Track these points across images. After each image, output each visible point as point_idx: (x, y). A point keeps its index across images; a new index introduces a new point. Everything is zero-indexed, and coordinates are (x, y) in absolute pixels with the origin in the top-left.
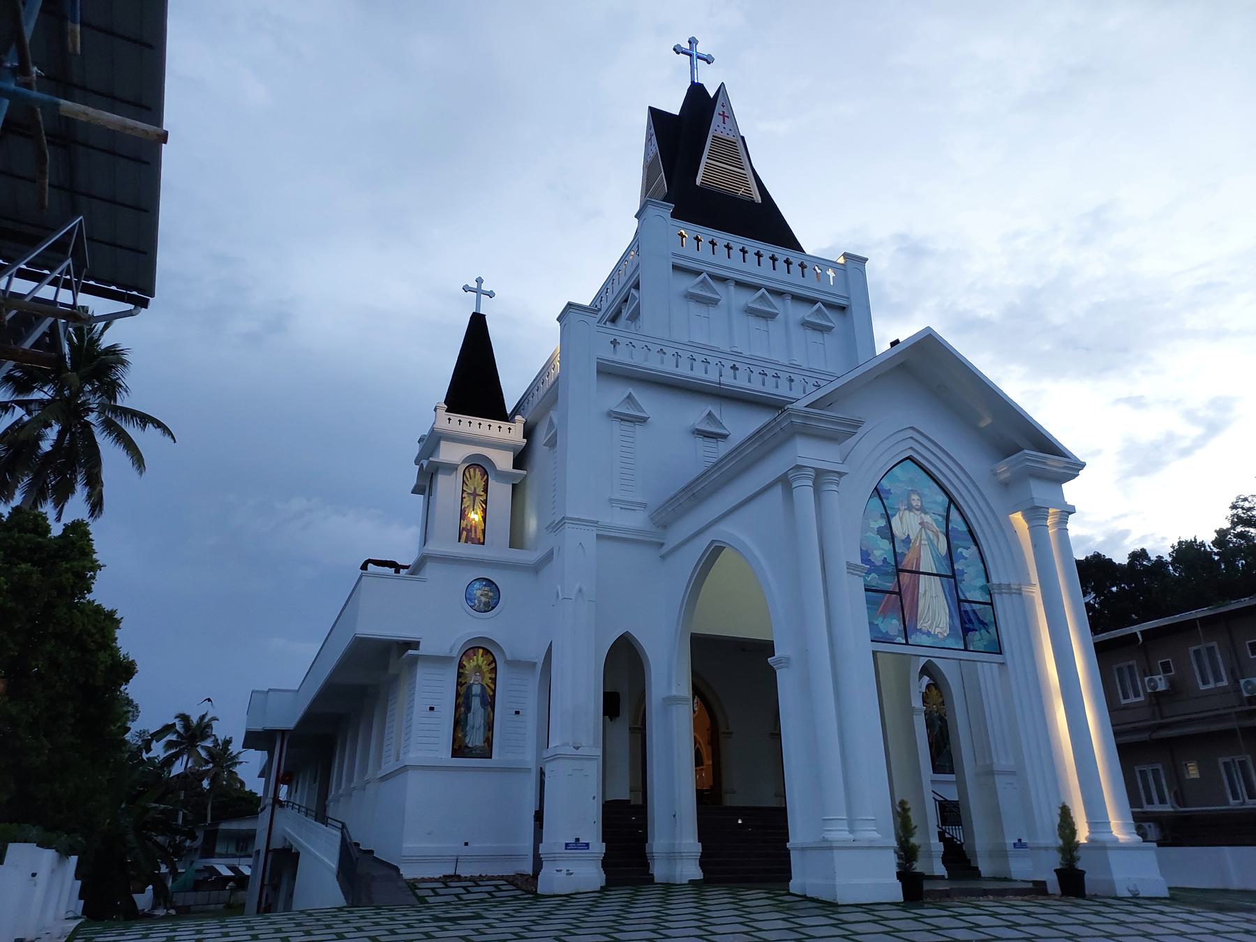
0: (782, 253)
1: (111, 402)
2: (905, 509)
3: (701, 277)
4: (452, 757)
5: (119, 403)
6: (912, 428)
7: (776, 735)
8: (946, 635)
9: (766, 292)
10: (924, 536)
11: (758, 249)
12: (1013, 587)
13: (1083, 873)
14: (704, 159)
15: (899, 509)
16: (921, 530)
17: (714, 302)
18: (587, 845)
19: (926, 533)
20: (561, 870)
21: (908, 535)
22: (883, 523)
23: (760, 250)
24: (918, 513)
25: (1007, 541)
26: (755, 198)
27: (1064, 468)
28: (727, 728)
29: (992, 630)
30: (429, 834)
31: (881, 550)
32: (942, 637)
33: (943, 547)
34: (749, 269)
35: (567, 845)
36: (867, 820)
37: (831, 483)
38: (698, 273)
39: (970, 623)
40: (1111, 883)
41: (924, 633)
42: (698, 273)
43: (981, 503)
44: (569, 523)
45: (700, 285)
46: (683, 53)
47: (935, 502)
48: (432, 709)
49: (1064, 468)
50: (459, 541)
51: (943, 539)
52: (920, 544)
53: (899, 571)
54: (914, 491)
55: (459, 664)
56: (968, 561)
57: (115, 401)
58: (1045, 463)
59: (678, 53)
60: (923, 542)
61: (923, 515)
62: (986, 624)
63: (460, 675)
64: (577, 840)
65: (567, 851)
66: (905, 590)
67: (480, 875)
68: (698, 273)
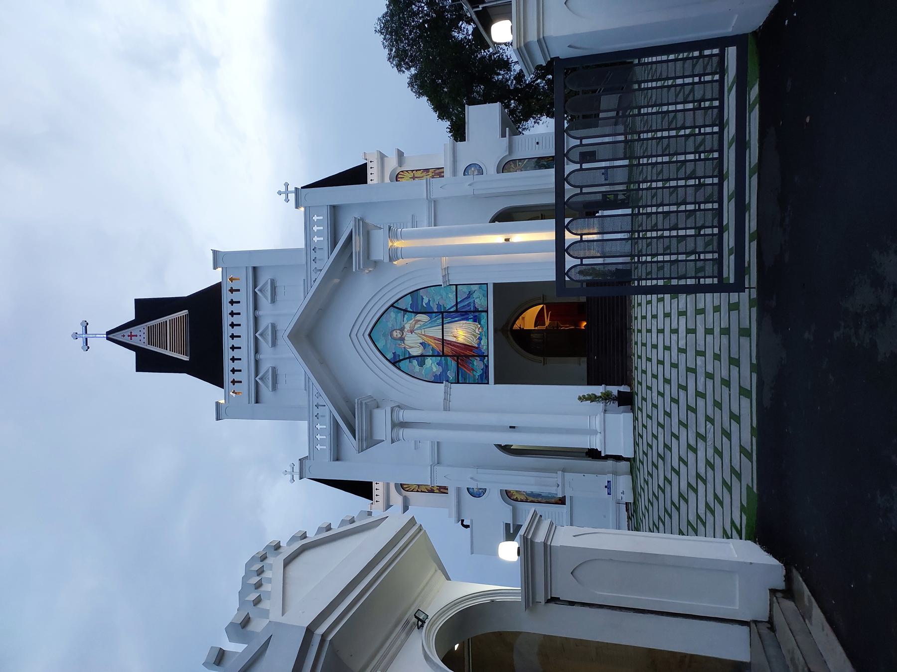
0: (226, 297)
2: (404, 343)
4: (565, 504)
8: (479, 326)
9: (258, 377)
10: (419, 331)
12: (444, 274)
14: (168, 353)
15: (404, 348)
17: (274, 370)
18: (608, 482)
19: (417, 329)
21: (421, 343)
22: (415, 362)
24: (405, 333)
27: (359, 235)
28: (540, 298)
32: (481, 328)
33: (423, 318)
34: (244, 307)
35: (609, 494)
38: (257, 383)
41: (480, 343)
42: (257, 383)
43: (391, 286)
45: (264, 380)
46: (87, 345)
49: (359, 235)
51: (420, 317)
52: (423, 335)
53: (444, 355)
54: (391, 335)
55: (515, 501)
59: (88, 348)
61: (406, 330)
62: (470, 292)
63: (522, 501)
64: (606, 487)
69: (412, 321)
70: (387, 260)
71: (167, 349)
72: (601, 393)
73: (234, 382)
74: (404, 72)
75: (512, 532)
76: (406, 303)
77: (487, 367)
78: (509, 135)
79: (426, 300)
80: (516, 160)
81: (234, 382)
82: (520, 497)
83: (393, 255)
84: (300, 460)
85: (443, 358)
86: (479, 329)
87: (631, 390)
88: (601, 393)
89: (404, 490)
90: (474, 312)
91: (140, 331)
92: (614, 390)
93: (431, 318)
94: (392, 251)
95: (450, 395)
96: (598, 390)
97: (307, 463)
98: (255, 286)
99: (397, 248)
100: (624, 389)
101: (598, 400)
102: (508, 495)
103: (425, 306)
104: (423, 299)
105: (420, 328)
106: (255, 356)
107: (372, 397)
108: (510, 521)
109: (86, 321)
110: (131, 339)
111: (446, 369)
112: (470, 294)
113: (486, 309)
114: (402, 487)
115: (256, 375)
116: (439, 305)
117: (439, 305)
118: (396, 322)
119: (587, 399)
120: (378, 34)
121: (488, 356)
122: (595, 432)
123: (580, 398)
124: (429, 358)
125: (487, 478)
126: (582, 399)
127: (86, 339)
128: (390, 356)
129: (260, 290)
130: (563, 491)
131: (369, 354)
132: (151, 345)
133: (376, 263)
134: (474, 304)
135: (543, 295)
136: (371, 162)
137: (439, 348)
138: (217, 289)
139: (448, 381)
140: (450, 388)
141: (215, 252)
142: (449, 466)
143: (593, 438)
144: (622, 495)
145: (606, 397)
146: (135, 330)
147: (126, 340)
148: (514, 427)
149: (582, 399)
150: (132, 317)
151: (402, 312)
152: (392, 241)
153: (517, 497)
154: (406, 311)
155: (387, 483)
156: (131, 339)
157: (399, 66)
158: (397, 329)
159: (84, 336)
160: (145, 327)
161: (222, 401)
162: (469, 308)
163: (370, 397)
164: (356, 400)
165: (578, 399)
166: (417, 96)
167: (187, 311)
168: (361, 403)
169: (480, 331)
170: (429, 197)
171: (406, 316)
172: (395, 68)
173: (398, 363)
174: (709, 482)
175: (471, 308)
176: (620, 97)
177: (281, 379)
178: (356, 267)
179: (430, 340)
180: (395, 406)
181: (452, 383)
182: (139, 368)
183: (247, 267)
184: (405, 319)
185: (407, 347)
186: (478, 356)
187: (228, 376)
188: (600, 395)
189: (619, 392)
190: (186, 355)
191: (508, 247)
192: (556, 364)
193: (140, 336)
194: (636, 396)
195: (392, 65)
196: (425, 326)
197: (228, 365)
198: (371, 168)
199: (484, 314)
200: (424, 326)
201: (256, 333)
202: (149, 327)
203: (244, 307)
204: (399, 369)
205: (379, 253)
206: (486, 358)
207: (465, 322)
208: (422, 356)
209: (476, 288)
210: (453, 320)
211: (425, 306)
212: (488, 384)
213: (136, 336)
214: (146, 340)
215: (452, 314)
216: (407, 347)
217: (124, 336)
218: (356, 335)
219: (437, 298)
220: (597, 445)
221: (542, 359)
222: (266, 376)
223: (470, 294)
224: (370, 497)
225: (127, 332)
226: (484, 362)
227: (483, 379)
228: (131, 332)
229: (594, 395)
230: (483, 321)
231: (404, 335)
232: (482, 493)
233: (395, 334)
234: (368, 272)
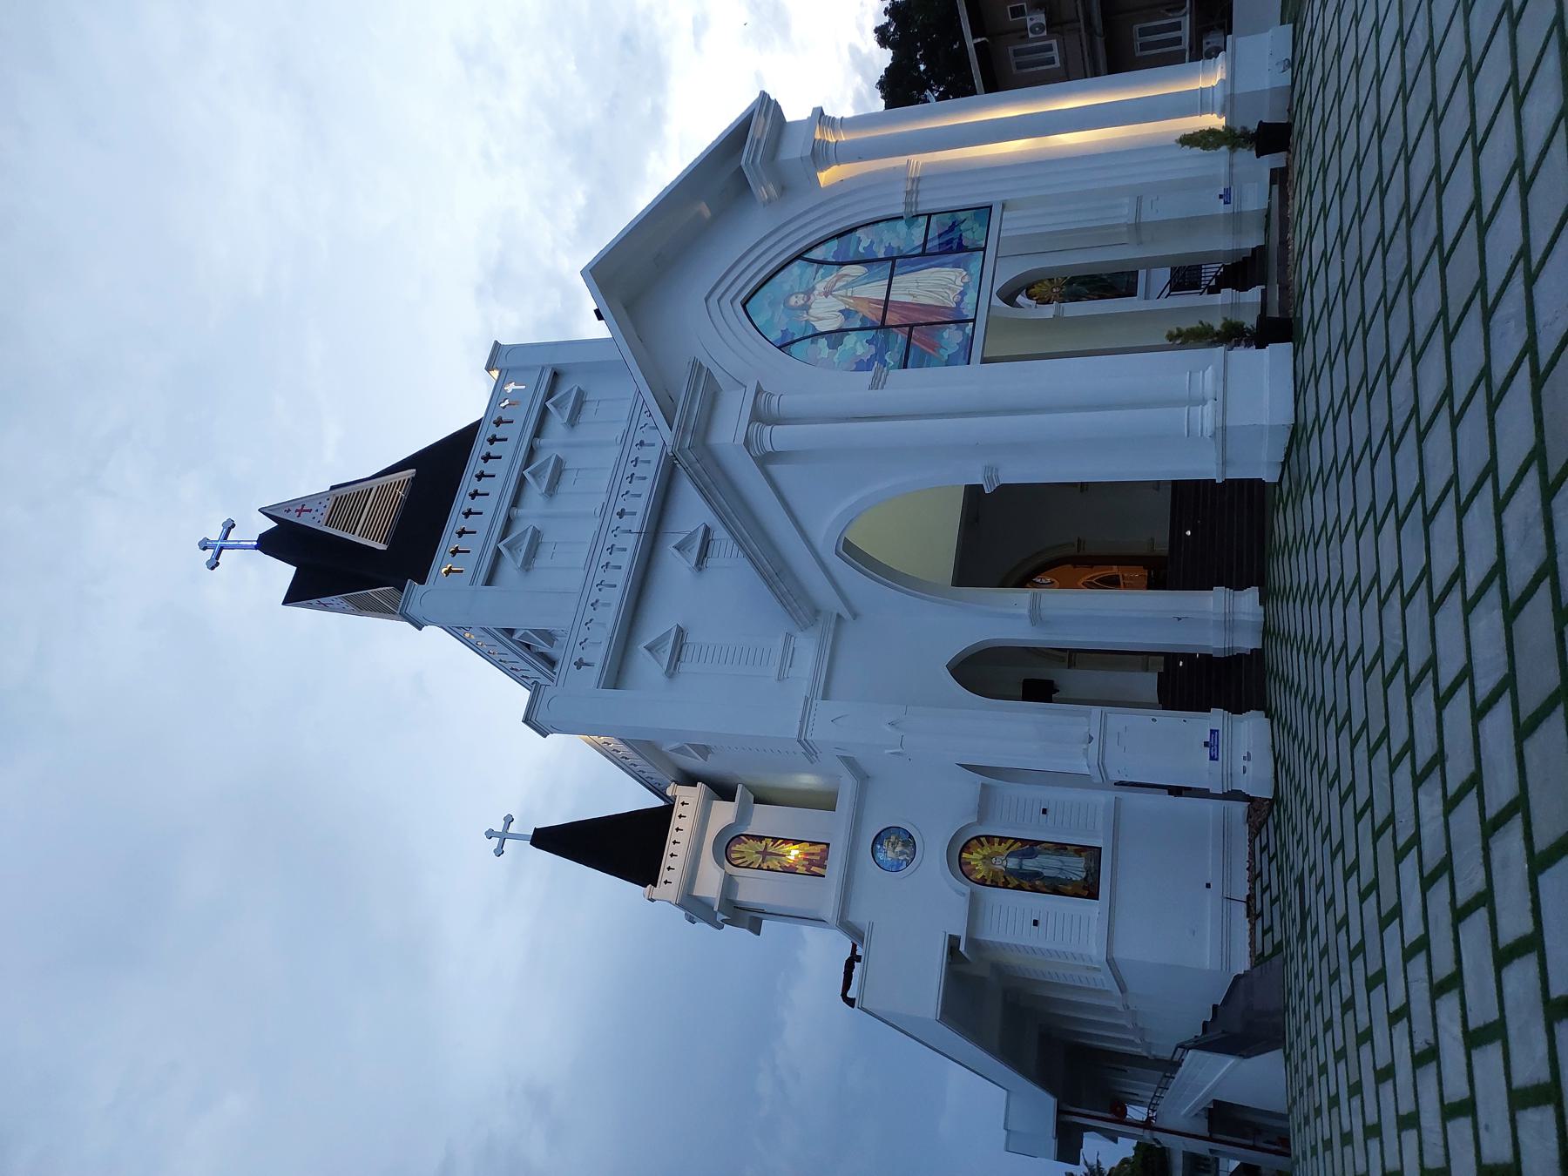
0: (480, 447)
4: (1098, 899)
7: (1083, 486)
8: (965, 273)
9: (551, 401)
10: (842, 292)
14: (355, 538)
16: (834, 296)
17: (537, 534)
18: (1212, 732)
21: (840, 311)
24: (812, 297)
29: (962, 216)
31: (856, 345)
34: (498, 488)
35: (1212, 758)
37: (764, 448)
38: (498, 553)
39: (952, 242)
40: (1274, 91)
41: (962, 300)
42: (498, 553)
46: (218, 558)
47: (801, 276)
51: (847, 269)
52: (850, 297)
54: (786, 302)
59: (218, 564)
60: (849, 294)
61: (816, 292)
62: (954, 223)
64: (1206, 744)
80: (994, 837)
89: (728, 860)
106: (509, 510)
115: (504, 536)
135: (1079, 540)
144: (1245, 763)
158: (798, 293)
174: (1470, 1010)
175: (952, 247)
177: (545, 552)
178: (747, 159)
185: (812, 319)
201: (503, 538)
203: (498, 488)
209: (962, 216)
210: (913, 268)
213: (310, 511)
216: (812, 319)
218: (719, 301)
222: (518, 545)
226: (964, 331)
231: (809, 303)
232: (905, 862)
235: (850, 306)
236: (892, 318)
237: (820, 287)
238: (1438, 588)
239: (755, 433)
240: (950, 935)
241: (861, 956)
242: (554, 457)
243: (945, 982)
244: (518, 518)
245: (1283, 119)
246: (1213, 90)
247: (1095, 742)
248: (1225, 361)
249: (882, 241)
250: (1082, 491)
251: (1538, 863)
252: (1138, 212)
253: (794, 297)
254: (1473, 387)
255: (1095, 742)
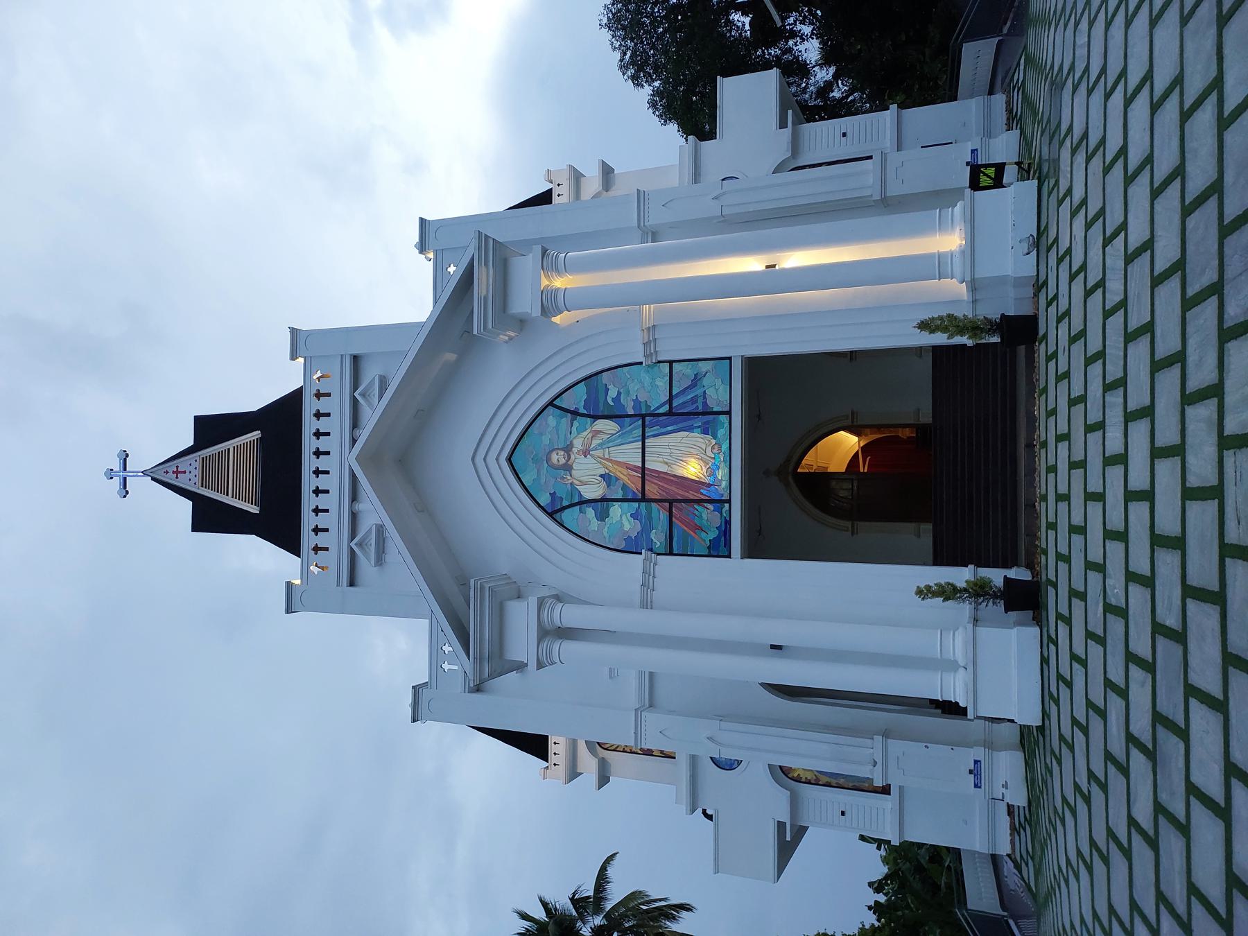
0: (310, 405)
1: (591, 902)
2: (571, 475)
3: (355, 548)
4: (890, 794)
5: (591, 893)
6: (473, 459)
7: (852, 355)
8: (714, 442)
9: (355, 541)
10: (599, 453)
11: (311, 454)
13: (1003, 315)
14: (229, 500)
15: (571, 484)
16: (593, 456)
18: (976, 762)
19: (596, 449)
20: (1003, 793)
21: (601, 476)
22: (590, 512)
23: (312, 393)
24: (572, 457)
25: (587, 337)
26: (257, 437)
27: (486, 264)
28: (847, 416)
29: (704, 367)
30: (966, 824)
31: (622, 518)
32: (716, 447)
35: (976, 786)
36: (941, 650)
37: (552, 618)
39: (696, 402)
40: (1018, 282)
42: (352, 554)
44: (641, 745)
45: (365, 547)
46: (125, 487)
47: (557, 428)
48: (843, 813)
49: (486, 264)
50: (674, 758)
51: (601, 424)
53: (644, 499)
54: (549, 459)
56: (621, 391)
57: (588, 897)
58: (486, 298)
59: (127, 493)
60: (607, 456)
61: (575, 450)
62: (696, 375)
63: (809, 782)
64: (971, 772)
65: (983, 787)
66: (666, 493)
67: (1006, 124)
68: (352, 554)
69: (585, 434)
70: (536, 312)
71: (227, 495)
72: (966, 582)
73: (316, 549)
74: (642, 86)
75: (788, 839)
76: (577, 399)
77: (728, 523)
78: (794, 124)
79: (613, 393)
81: (316, 549)
82: (803, 776)
83: (550, 304)
84: (413, 687)
85: (643, 504)
86: (713, 448)
87: (1033, 577)
88: (966, 582)
90: (704, 414)
91: (190, 465)
92: (996, 576)
93: (622, 427)
94: (547, 295)
95: (654, 577)
96: (961, 576)
97: (425, 694)
98: (355, 384)
99: (557, 290)
100: (1018, 573)
101: (960, 597)
102: (784, 774)
103: (612, 404)
104: (607, 390)
105: (601, 446)
107: (509, 578)
108: (786, 818)
109: (125, 451)
110: (177, 478)
111: (648, 526)
112: (696, 380)
113: (727, 409)
114: (596, 746)
115: (353, 535)
116: (637, 402)
117: (637, 402)
118: (558, 434)
119: (935, 594)
120: (605, 30)
121: (729, 501)
122: (953, 666)
123: (919, 592)
124: (617, 505)
125: (733, 742)
126: (924, 593)
127: (125, 479)
128: (544, 500)
129: (363, 395)
130: (885, 773)
131: (506, 495)
132: (212, 490)
133: (522, 323)
134: (705, 398)
136: (559, 185)
137: (635, 486)
138: (296, 397)
139: (651, 550)
140: (655, 564)
141: (294, 332)
142: (671, 712)
143: (949, 678)
144: (1004, 790)
145: (979, 590)
146: (183, 464)
147: (170, 478)
148: (779, 647)
149: (924, 593)
150: (189, 441)
151: (569, 414)
152: (547, 277)
153: (799, 775)
154: (575, 413)
155: (574, 739)
156: (177, 478)
157: (634, 78)
158: (558, 449)
159: (121, 474)
160: (198, 459)
161: (298, 582)
162: (695, 406)
163: (506, 577)
164: (472, 582)
165: (917, 594)
166: (662, 122)
167: (259, 432)
168: (482, 588)
169: (715, 451)
170: (642, 224)
171: (576, 424)
172: (630, 81)
173: (558, 514)
176: (1000, 43)
179: (620, 469)
180: (547, 597)
181: (659, 554)
182: (197, 527)
183: (342, 356)
184: (574, 429)
186: (711, 501)
187: (308, 539)
188: (964, 585)
189: (1006, 579)
190: (255, 505)
191: (773, 280)
192: (871, 532)
193: (190, 472)
194: (1051, 591)
195: (626, 77)
196: (610, 442)
197: (308, 520)
198: (559, 195)
199: (724, 418)
200: (609, 442)
202: (203, 458)
204: (561, 525)
205: (524, 303)
206: (727, 505)
207: (686, 433)
208: (604, 500)
210: (663, 430)
211: (612, 404)
212: (730, 557)
213: (184, 472)
214: (198, 480)
215: (661, 418)
217: (167, 472)
218: (485, 459)
219: (634, 387)
220: (957, 693)
221: (849, 524)
223: (696, 380)
224: (543, 755)
225: (172, 467)
226: (721, 514)
227: (719, 548)
228: (177, 467)
229: (952, 585)
230: (722, 432)
232: (736, 762)
233: (554, 457)
234: (507, 338)
235: (610, 471)
236: (652, 490)
237: (578, 444)
238: (1159, 90)
239: (550, 303)
240: (778, 821)
241: (712, 815)
242: (377, 378)
243: (778, 844)
244: (361, 512)
245: (1026, 310)
246: (952, 256)
247: (879, 766)
248: (974, 639)
249: (628, 393)
250: (851, 359)
251: (1226, 230)
252: (884, 182)
253: (555, 453)
254: (1225, 752)
255: (879, 766)
